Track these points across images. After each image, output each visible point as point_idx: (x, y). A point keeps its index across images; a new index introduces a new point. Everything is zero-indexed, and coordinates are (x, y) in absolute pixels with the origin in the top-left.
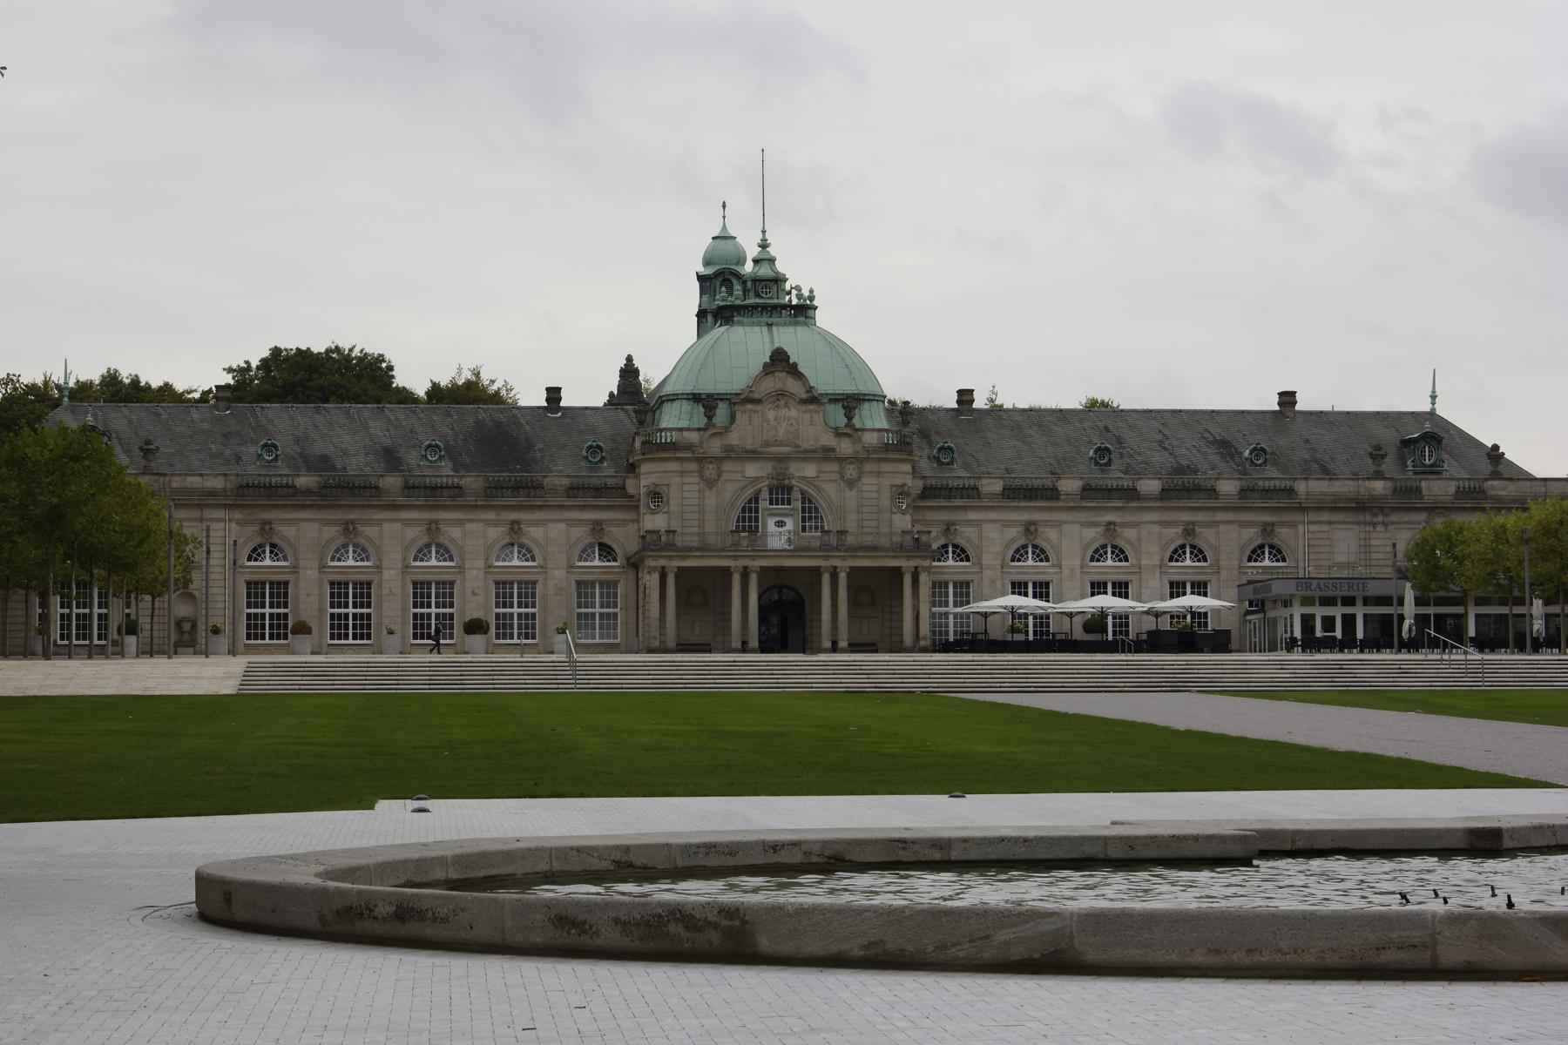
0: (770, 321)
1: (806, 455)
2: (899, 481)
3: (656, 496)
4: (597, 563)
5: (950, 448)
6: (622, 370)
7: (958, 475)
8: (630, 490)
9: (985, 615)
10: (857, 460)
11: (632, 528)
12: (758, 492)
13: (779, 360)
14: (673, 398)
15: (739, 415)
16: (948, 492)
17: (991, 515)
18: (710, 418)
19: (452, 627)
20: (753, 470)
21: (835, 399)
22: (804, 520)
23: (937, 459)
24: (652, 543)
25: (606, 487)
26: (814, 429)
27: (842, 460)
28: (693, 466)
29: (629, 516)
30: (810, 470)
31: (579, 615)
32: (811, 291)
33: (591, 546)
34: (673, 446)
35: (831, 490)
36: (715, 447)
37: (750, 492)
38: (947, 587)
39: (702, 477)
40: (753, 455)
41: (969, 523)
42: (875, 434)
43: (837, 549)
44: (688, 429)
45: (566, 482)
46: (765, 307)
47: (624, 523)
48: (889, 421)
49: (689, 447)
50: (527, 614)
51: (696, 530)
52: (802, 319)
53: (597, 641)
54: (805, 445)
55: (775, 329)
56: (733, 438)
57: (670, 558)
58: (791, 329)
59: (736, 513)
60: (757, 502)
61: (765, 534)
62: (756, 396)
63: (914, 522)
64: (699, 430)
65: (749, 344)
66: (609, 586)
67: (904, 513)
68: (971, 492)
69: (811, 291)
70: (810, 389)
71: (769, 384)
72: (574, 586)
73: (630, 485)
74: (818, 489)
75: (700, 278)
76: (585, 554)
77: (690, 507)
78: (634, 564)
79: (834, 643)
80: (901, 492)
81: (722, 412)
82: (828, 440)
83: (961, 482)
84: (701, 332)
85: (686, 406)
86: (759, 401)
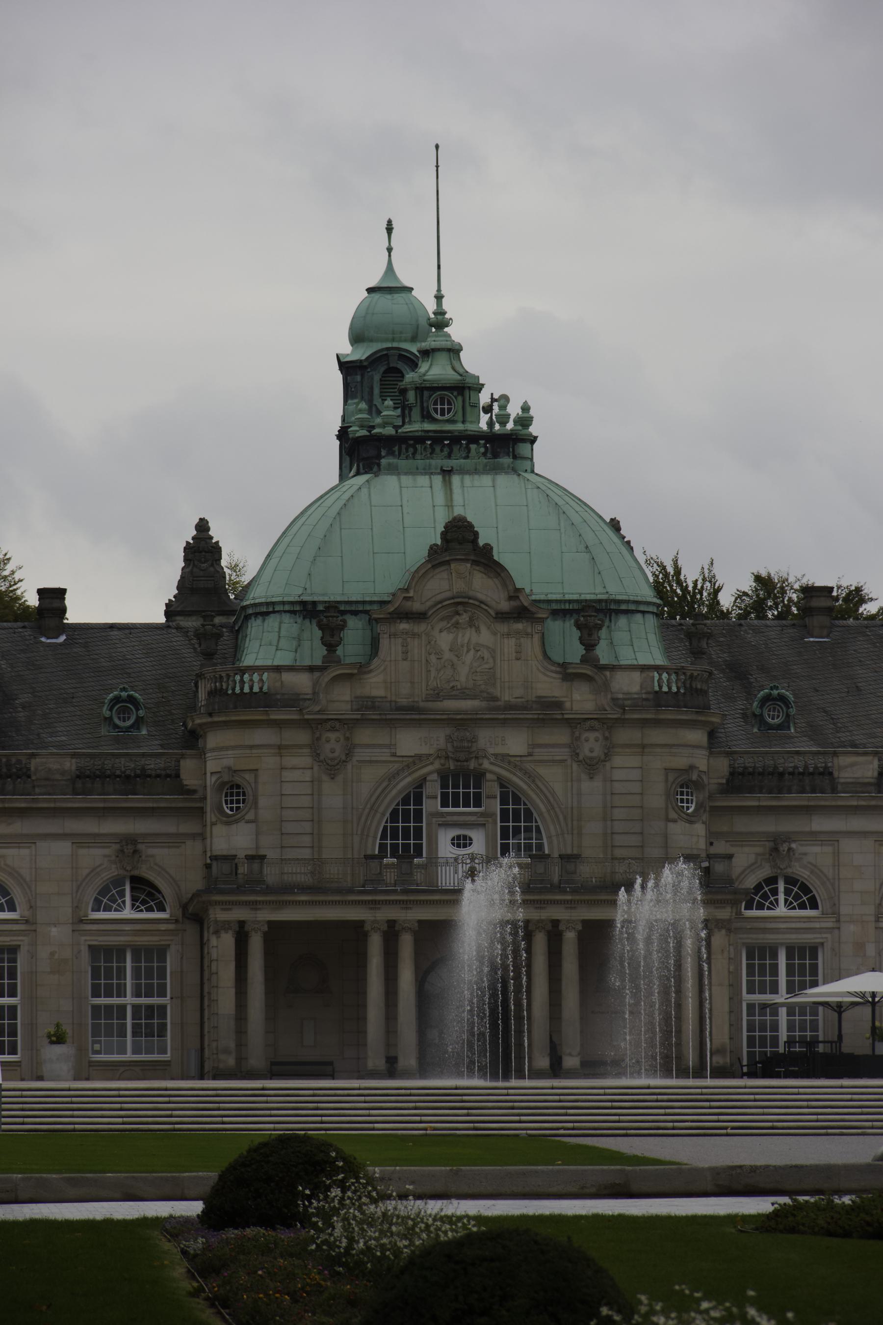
0: (448, 464)
1: (507, 715)
2: (681, 762)
3: (235, 790)
4: (128, 913)
5: (782, 698)
6: (188, 548)
7: (798, 748)
8: (189, 779)
9: (839, 1008)
10: (604, 723)
11: (192, 849)
12: (421, 784)
13: (459, 541)
14: (267, 610)
15: (384, 642)
16: (776, 779)
17: (857, 823)
18: (331, 647)
19: (13, 1033)
20: (410, 742)
21: (563, 610)
22: (505, 834)
23: (760, 719)
24: (229, 877)
25: (144, 775)
26: (521, 667)
27: (574, 724)
28: (302, 737)
29: (188, 827)
30: (515, 743)
31: (96, 1009)
32: (526, 408)
33: (118, 882)
34: (264, 700)
35: (554, 778)
36: (341, 699)
37: (406, 782)
38: (774, 956)
39: (316, 755)
40: (410, 715)
41: (814, 837)
42: (636, 676)
43: (558, 888)
44: (291, 669)
45: (70, 765)
46: (438, 439)
47: (175, 840)
48: (667, 651)
49: (294, 701)
50: (150, 1008)
51: (306, 853)
52: (506, 461)
53: (129, 1056)
54: (507, 697)
55: (456, 480)
56: (374, 685)
57: (254, 905)
58: (486, 480)
59: (381, 822)
60: (419, 801)
61: (433, 860)
62: (417, 606)
63: (712, 837)
64: (311, 669)
65: (413, 504)
66: (151, 956)
67: (690, 820)
68: (820, 779)
69: (526, 408)
70: (515, 594)
71: (439, 586)
72: (85, 955)
73: (188, 769)
74: (532, 777)
75: (345, 366)
76: (106, 897)
77: (292, 811)
78: (194, 915)
79: (392, 1061)
80: (685, 782)
81: (354, 633)
82: (548, 686)
83: (798, 762)
84: (343, 477)
85: (289, 625)
86: (421, 617)
